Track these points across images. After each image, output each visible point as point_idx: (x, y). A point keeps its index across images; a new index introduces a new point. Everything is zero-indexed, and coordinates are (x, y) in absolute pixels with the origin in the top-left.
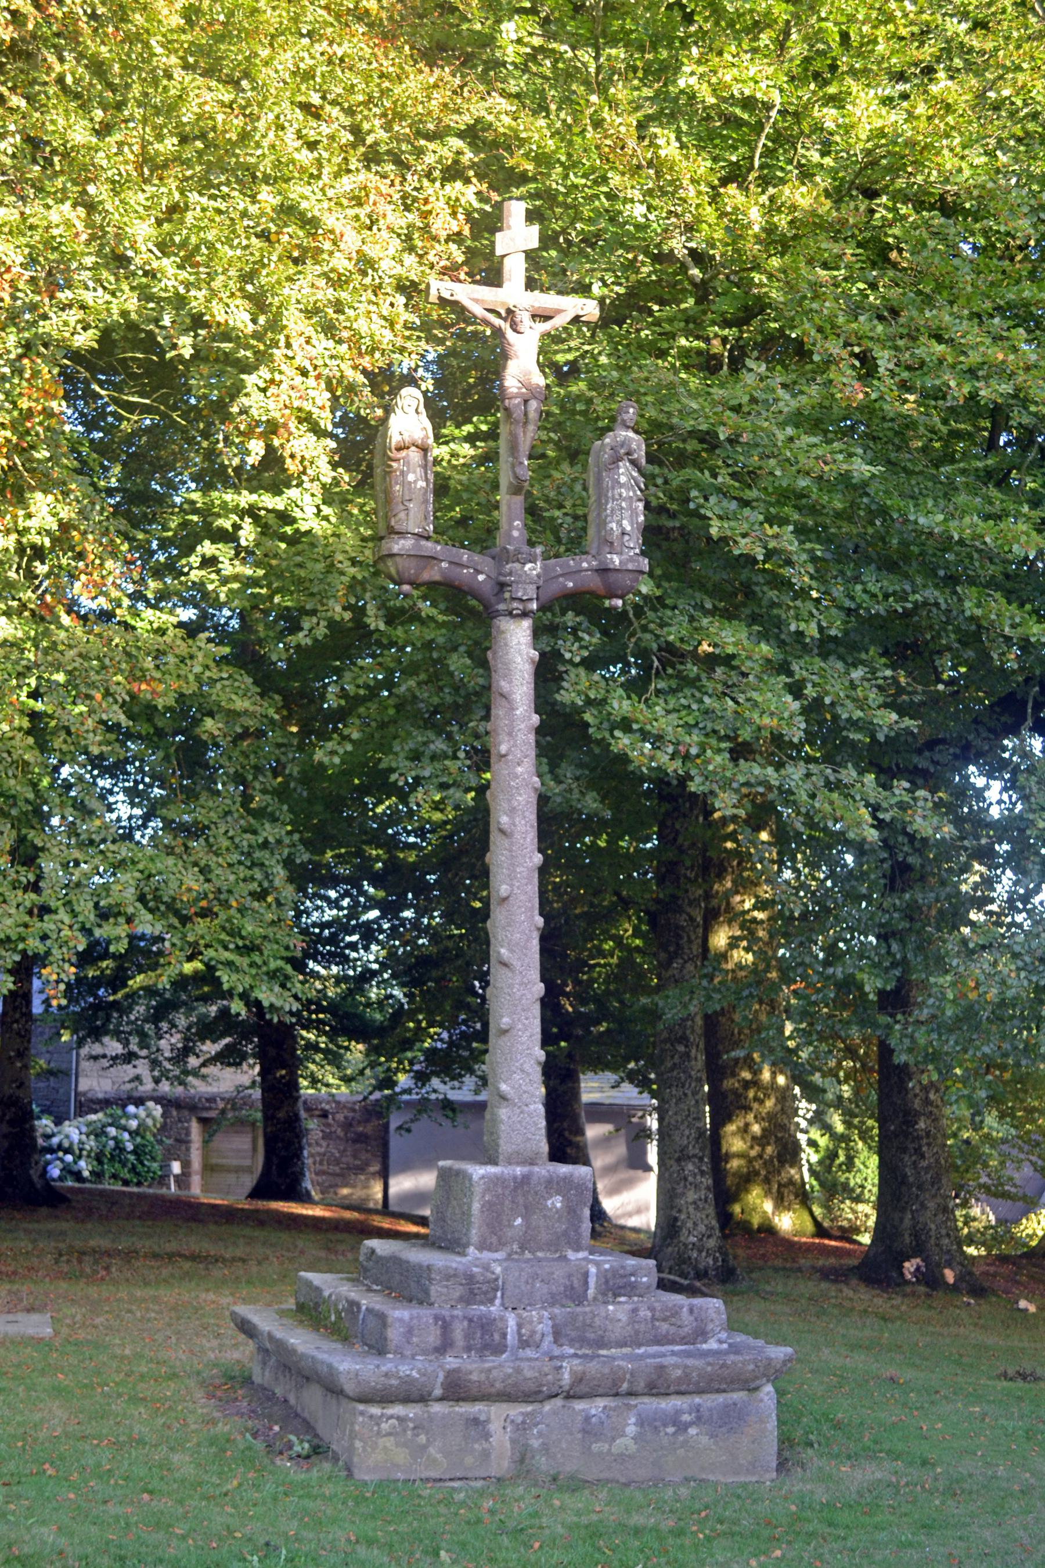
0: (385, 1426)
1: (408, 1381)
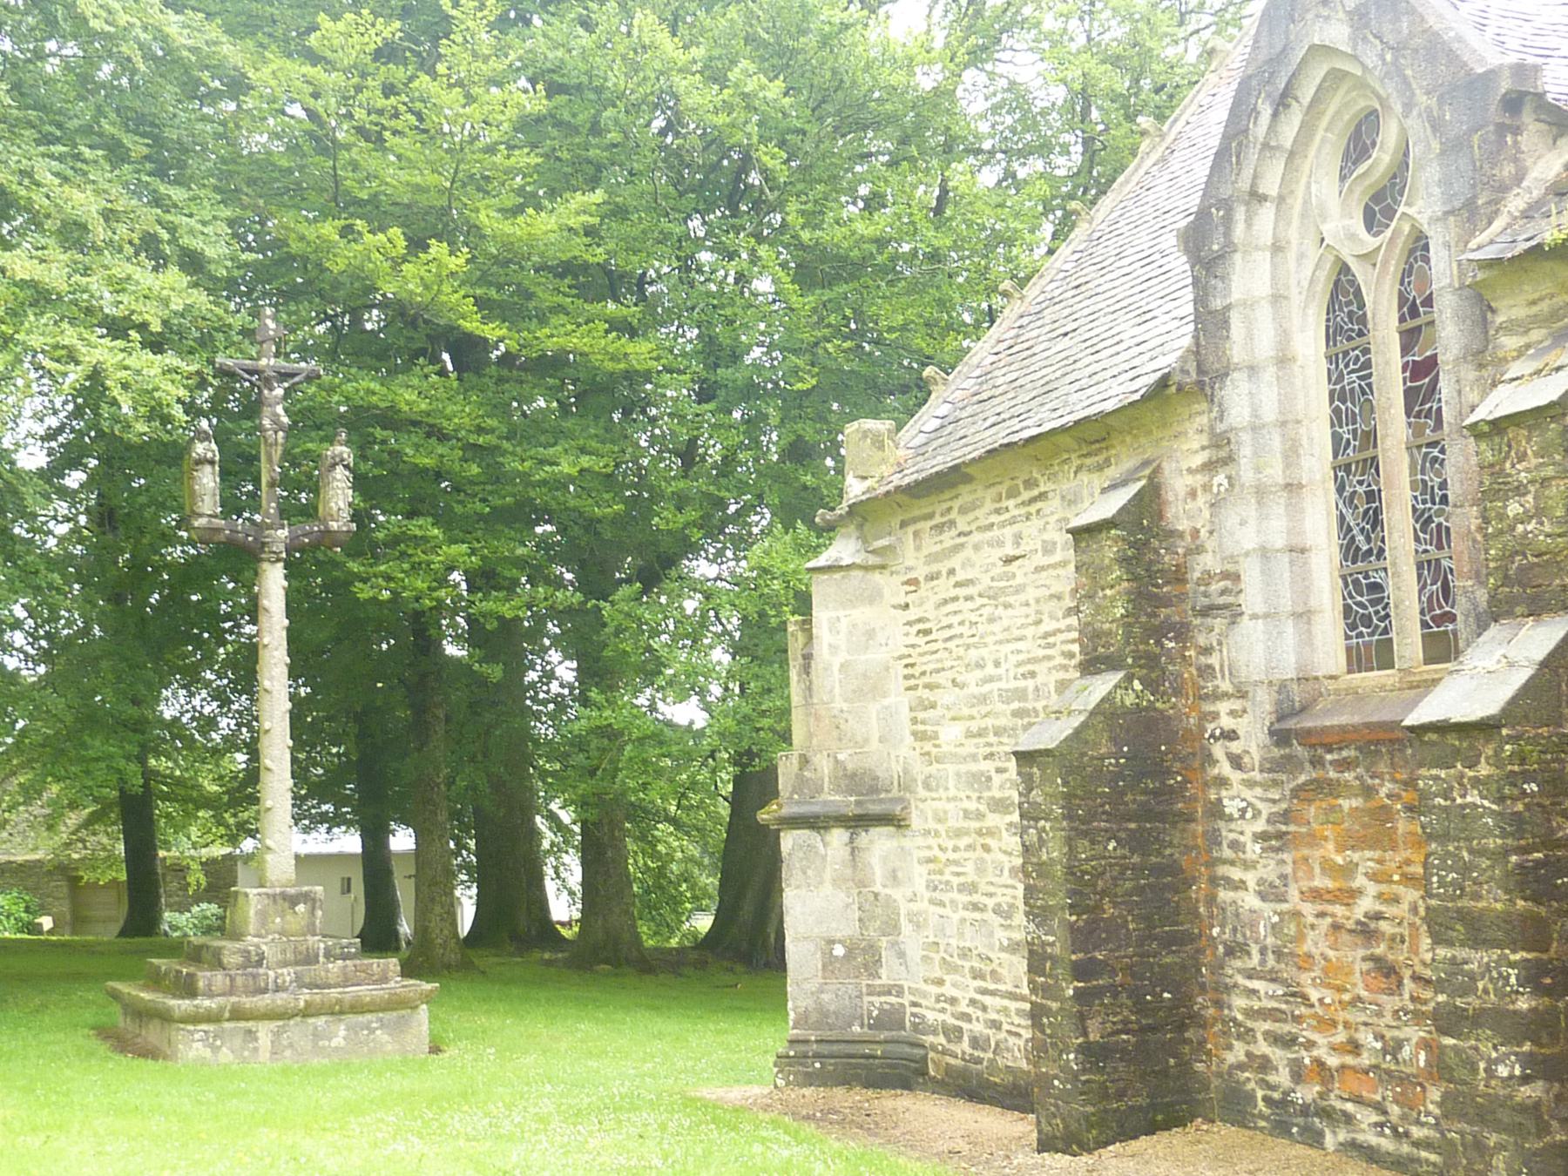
0: (197, 1036)
1: (209, 1010)
